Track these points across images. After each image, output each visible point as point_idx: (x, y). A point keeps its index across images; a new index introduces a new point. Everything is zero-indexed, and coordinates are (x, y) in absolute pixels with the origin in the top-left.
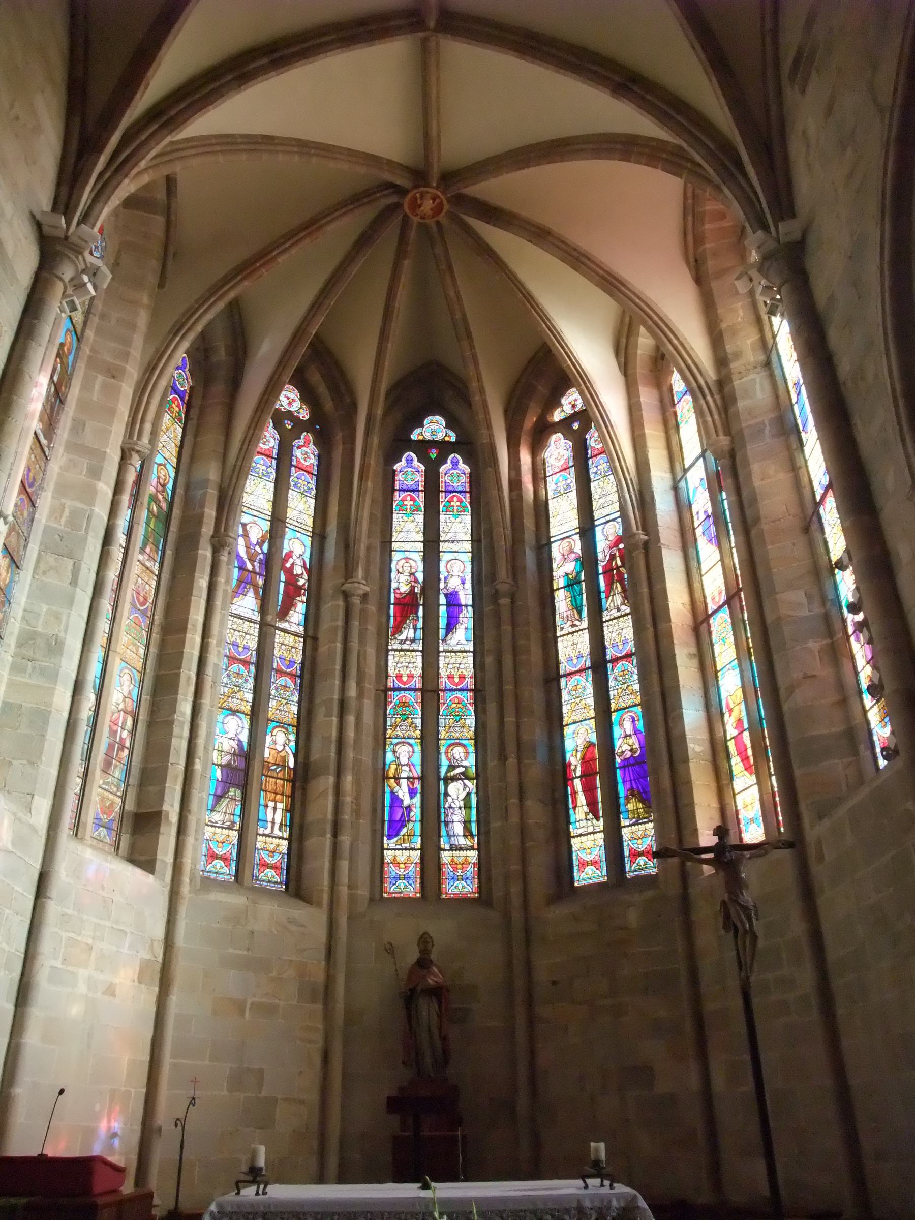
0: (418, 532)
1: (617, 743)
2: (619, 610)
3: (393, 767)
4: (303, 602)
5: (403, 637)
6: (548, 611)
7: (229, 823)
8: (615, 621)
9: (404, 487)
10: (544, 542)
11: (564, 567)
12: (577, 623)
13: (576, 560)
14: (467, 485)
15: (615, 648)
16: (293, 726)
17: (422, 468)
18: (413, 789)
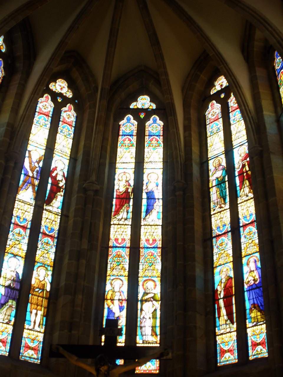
0: (132, 158)
1: (245, 276)
2: (247, 196)
3: (110, 293)
4: (61, 196)
5: (119, 217)
7: (7, 321)
8: (245, 202)
9: (125, 134)
10: (205, 160)
11: (216, 174)
12: (223, 206)
13: (223, 169)
14: (162, 132)
15: (245, 219)
16: (51, 266)
17: (136, 123)
18: (121, 307)
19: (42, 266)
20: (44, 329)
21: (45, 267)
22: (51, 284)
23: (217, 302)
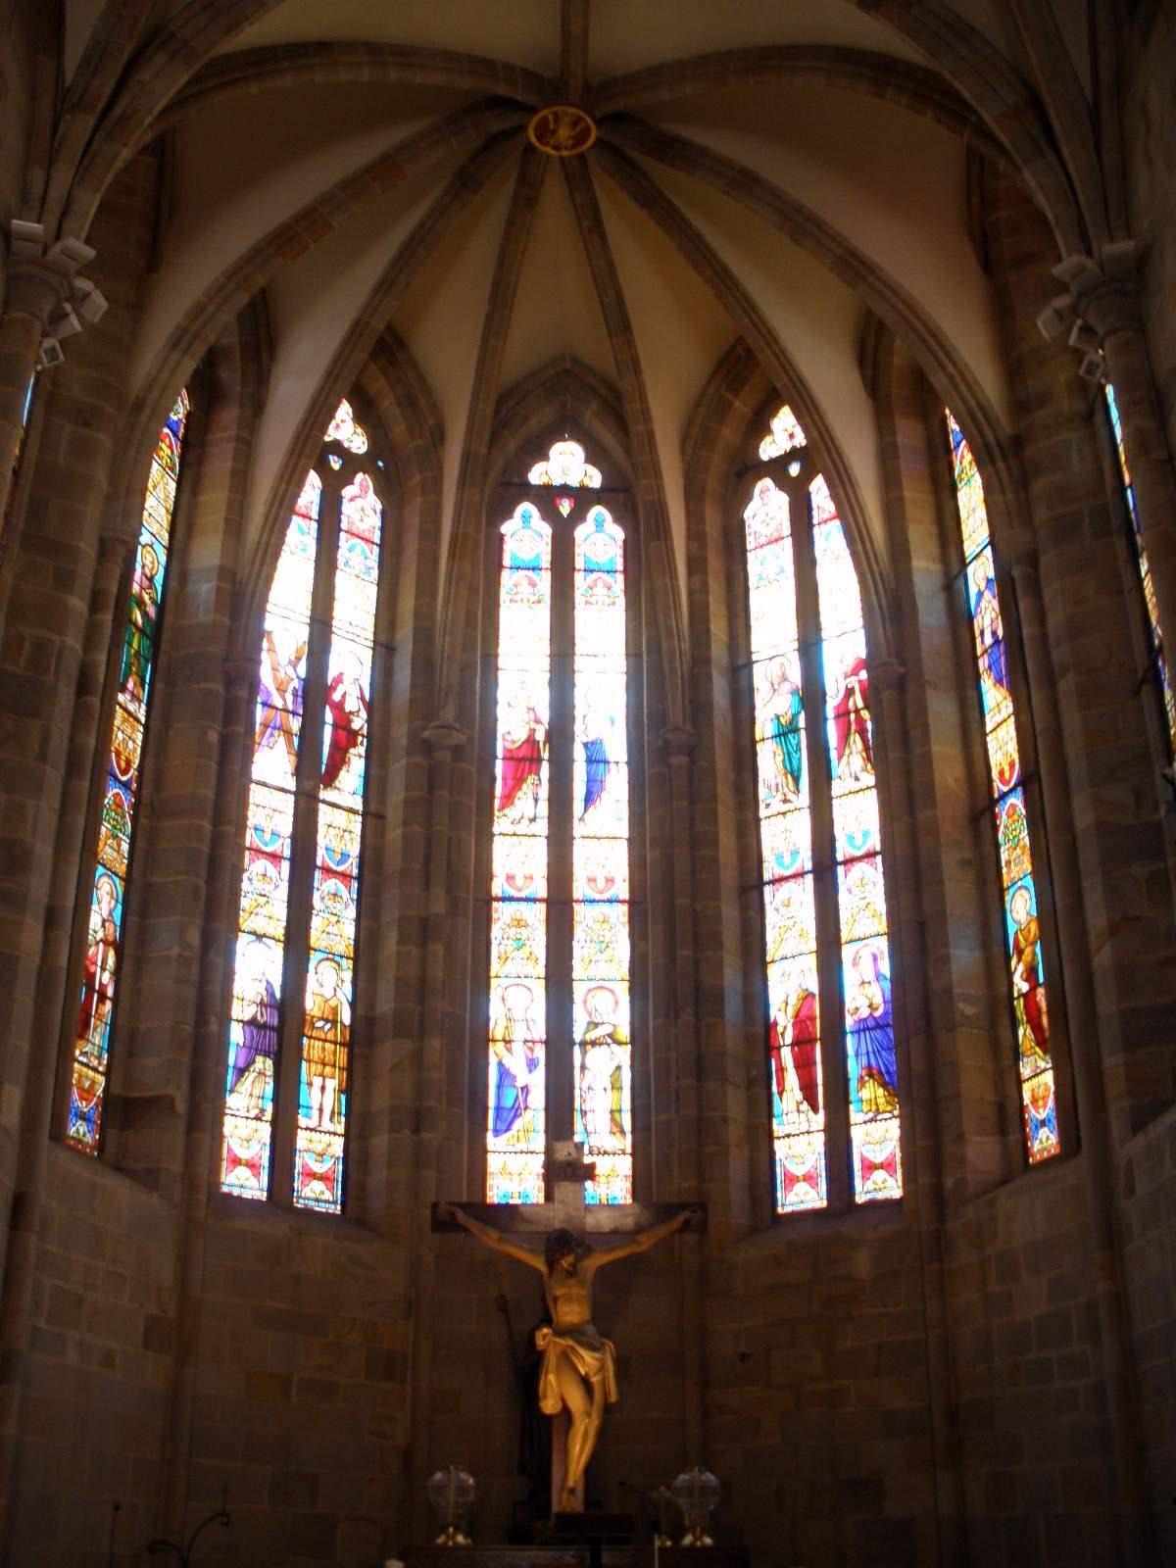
2: (857, 779)
4: (360, 756)
6: (747, 776)
7: (257, 1111)
10: (741, 661)
11: (773, 700)
12: (791, 796)
13: (794, 692)
16: (347, 958)
19: (328, 959)
20: (343, 1125)
21: (336, 962)
22: (353, 1005)
23: (774, 1053)
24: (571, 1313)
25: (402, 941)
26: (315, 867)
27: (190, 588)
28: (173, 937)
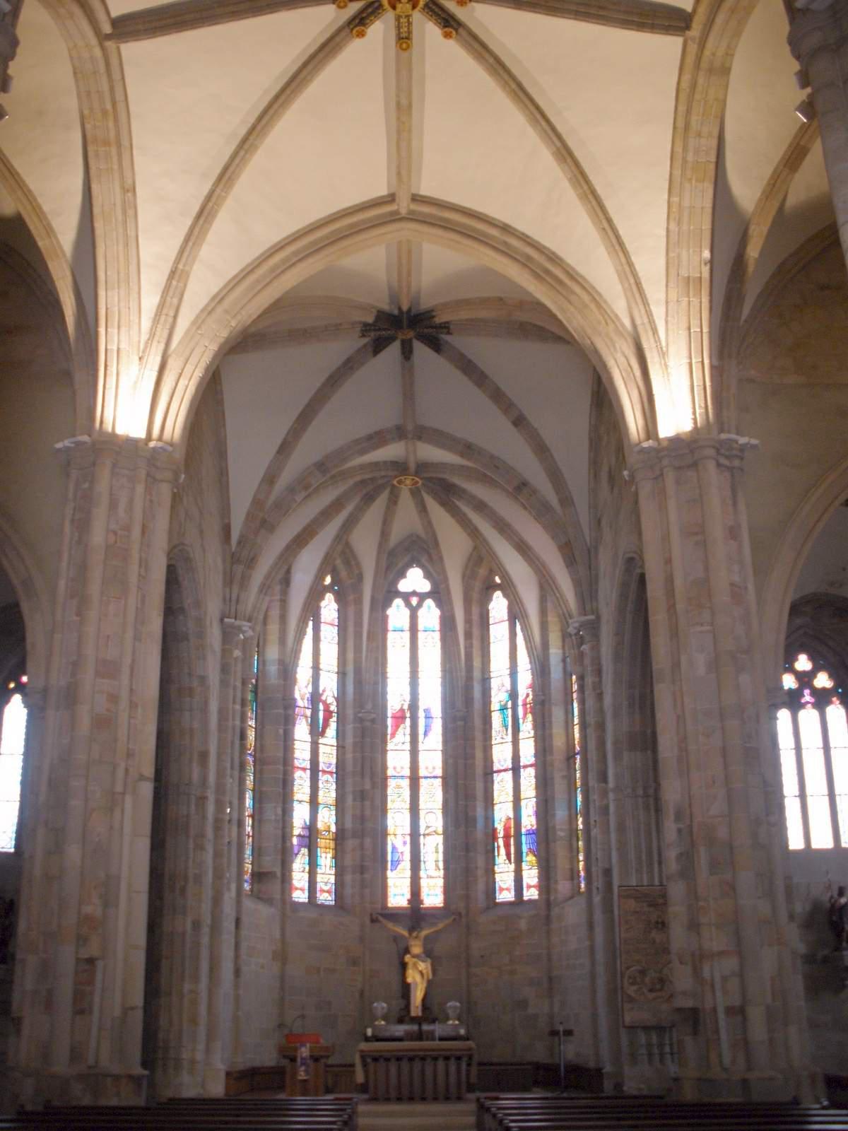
6: (488, 727)
10: (486, 677)
11: (499, 696)
12: (505, 737)
22: (336, 823)
24: (417, 949)
25: (354, 800)
26: (319, 771)
27: (267, 668)
28: (272, 811)
